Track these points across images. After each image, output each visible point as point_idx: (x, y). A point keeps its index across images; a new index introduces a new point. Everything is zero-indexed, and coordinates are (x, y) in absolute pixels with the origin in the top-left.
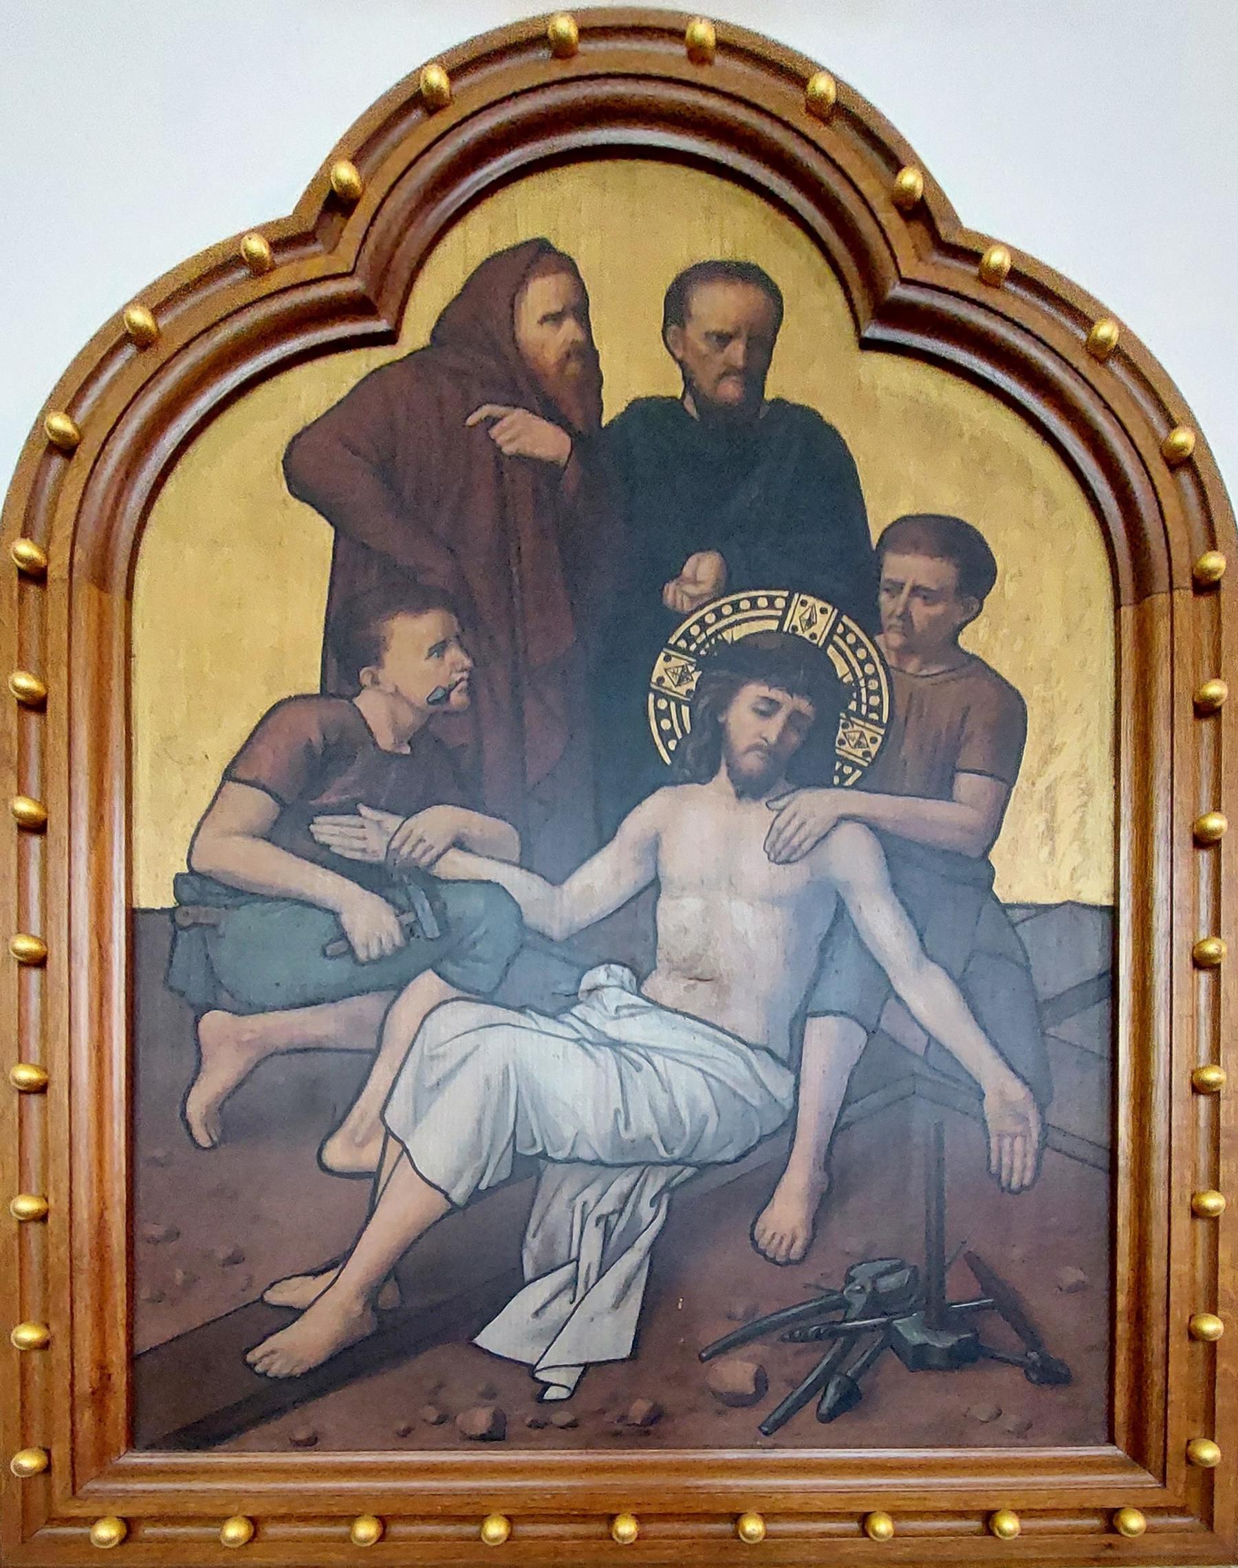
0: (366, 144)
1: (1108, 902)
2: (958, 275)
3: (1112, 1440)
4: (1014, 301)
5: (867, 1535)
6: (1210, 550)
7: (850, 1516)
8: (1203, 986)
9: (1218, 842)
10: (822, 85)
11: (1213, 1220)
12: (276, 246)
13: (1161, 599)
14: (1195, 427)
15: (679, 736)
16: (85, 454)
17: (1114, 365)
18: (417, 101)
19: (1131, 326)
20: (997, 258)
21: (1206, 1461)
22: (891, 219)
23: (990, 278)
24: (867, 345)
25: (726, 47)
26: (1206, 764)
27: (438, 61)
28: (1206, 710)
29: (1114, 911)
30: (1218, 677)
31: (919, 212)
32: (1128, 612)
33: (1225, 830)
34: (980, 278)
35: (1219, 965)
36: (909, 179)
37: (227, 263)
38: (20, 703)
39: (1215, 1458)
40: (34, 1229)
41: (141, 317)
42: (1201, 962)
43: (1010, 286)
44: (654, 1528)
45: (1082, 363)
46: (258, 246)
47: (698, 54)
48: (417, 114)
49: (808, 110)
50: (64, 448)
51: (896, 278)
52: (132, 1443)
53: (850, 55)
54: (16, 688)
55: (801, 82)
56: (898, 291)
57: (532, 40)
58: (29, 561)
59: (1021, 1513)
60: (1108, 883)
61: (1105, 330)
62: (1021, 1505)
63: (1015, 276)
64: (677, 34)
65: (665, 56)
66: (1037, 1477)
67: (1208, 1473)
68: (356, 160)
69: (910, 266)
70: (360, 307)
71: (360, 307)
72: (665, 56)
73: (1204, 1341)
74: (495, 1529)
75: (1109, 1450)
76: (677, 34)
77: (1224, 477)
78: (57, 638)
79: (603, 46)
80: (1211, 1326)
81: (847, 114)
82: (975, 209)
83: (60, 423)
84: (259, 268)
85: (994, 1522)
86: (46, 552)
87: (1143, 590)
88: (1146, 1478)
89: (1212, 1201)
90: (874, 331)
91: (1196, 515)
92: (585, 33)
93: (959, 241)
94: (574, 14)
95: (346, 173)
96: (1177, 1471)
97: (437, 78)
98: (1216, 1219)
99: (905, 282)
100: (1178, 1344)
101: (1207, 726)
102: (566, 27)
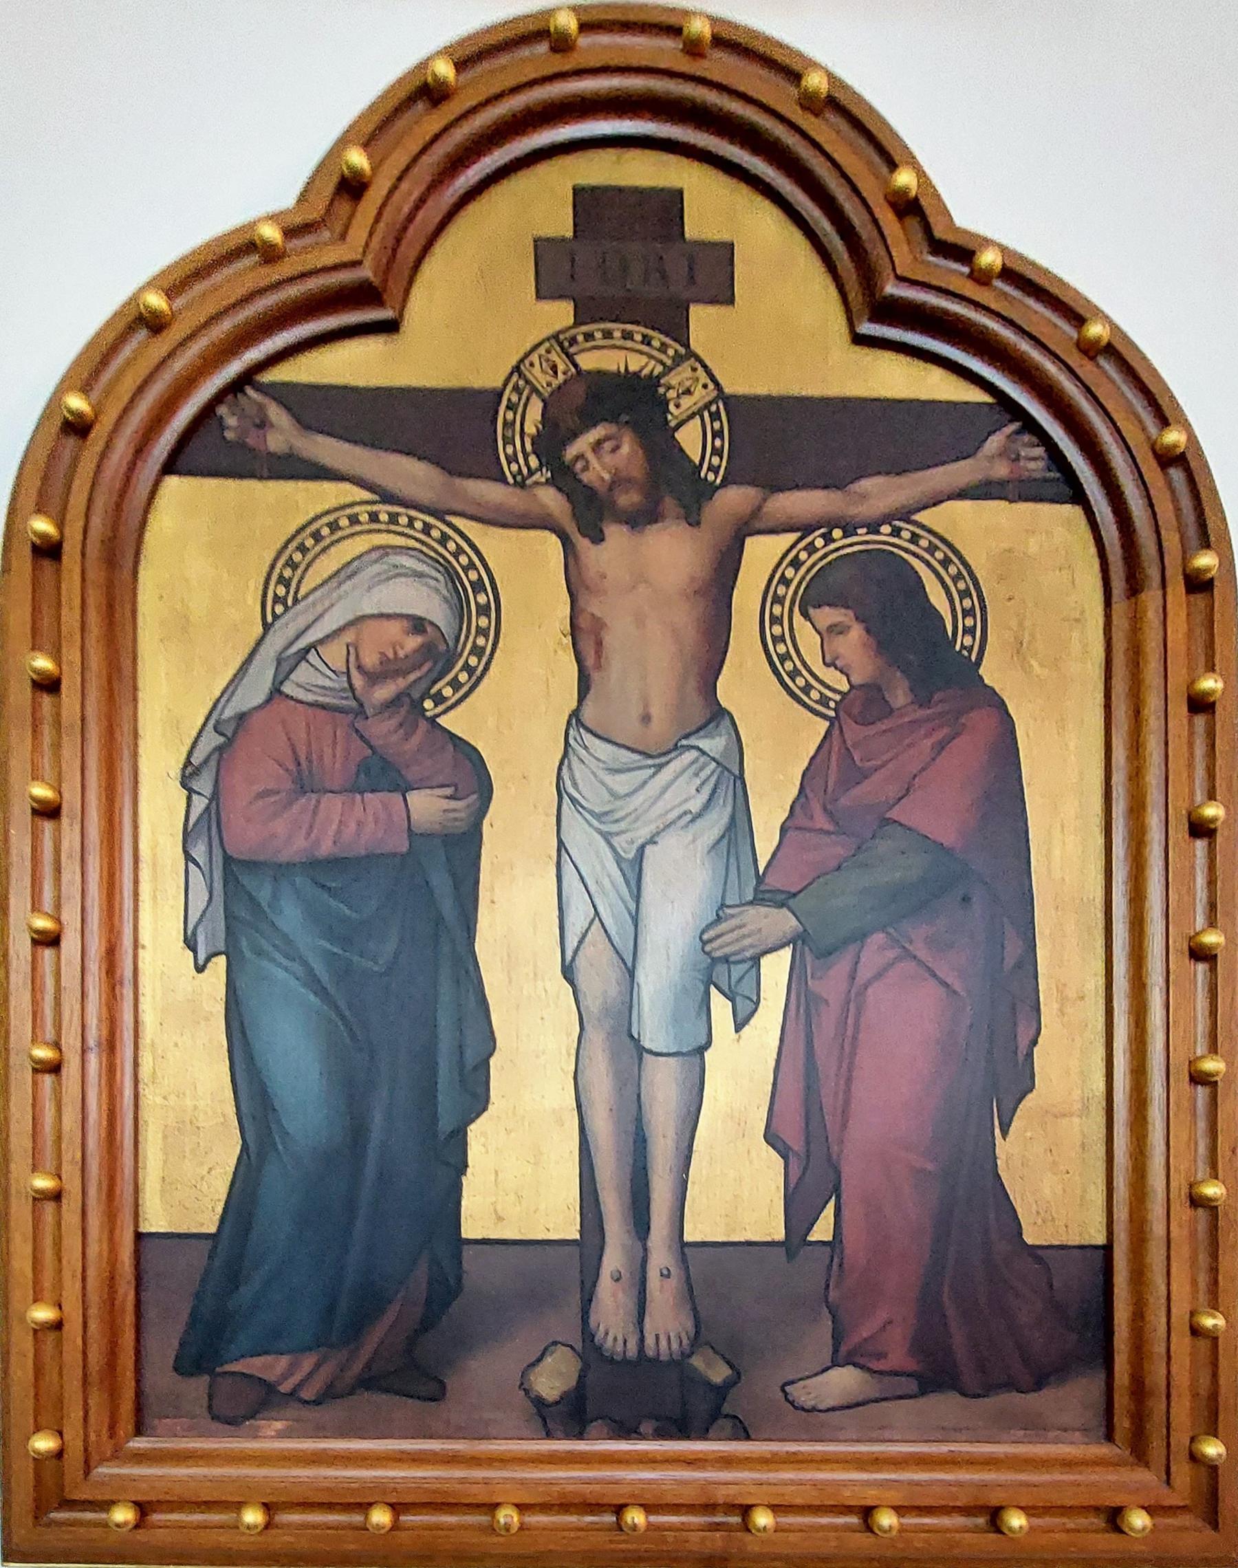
0: (377, 127)
1: (1100, 1239)
2: (952, 272)
3: (1109, 1437)
4: (825, 130)
5: (999, 1531)
6: (1203, 548)
7: (847, 1510)
8: (1200, 977)
9: (1210, 583)
10: (815, 81)
11: (1212, 1338)
12: (290, 233)
13: (1151, 598)
14: (1187, 427)
15: (706, 414)
16: (99, 434)
17: (1102, 361)
18: (424, 92)
19: (1125, 327)
20: (989, 259)
21: (1212, 1460)
22: (887, 218)
23: (982, 278)
24: (860, 340)
25: (719, 42)
26: (1200, 750)
27: (447, 51)
28: (1200, 705)
29: (1108, 1248)
30: (1213, 670)
31: (909, 208)
32: (1120, 606)
33: (1220, 692)
34: (971, 276)
35: (1216, 956)
36: (904, 178)
37: (243, 247)
38: (33, 681)
39: (1220, 1455)
40: (49, 1207)
41: (156, 301)
42: (1200, 954)
43: (998, 283)
44: (652, 1518)
45: (1074, 359)
46: (271, 233)
47: (694, 49)
48: (420, 106)
49: (803, 107)
50: (77, 428)
51: (892, 276)
52: (139, 1431)
53: (840, 46)
54: (35, 533)
55: (795, 77)
56: (892, 289)
57: (533, 33)
58: (43, 536)
59: (1027, 1510)
60: (1099, 1218)
61: (1095, 330)
62: (1141, 1503)
63: (1008, 274)
64: (674, 31)
65: (664, 50)
66: (1036, 1459)
67: (1213, 1468)
68: (366, 145)
69: (905, 265)
70: (365, 294)
71: (365, 294)
72: (664, 50)
73: (1208, 1337)
74: (380, 1517)
75: (1104, 1450)
76: (674, 31)
77: (1218, 488)
78: (71, 618)
79: (604, 39)
80: (1212, 1449)
81: (840, 106)
82: (969, 208)
83: (76, 402)
84: (270, 255)
85: (1002, 1520)
86: (60, 525)
87: (1134, 587)
88: (1147, 1477)
89: (1212, 1190)
90: (868, 328)
91: (1186, 502)
92: (584, 27)
93: (950, 238)
94: (575, 9)
95: (357, 158)
96: (1183, 1472)
97: (444, 69)
98: (1216, 1339)
99: (901, 279)
100: (1182, 1344)
101: (1200, 721)
102: (567, 22)
